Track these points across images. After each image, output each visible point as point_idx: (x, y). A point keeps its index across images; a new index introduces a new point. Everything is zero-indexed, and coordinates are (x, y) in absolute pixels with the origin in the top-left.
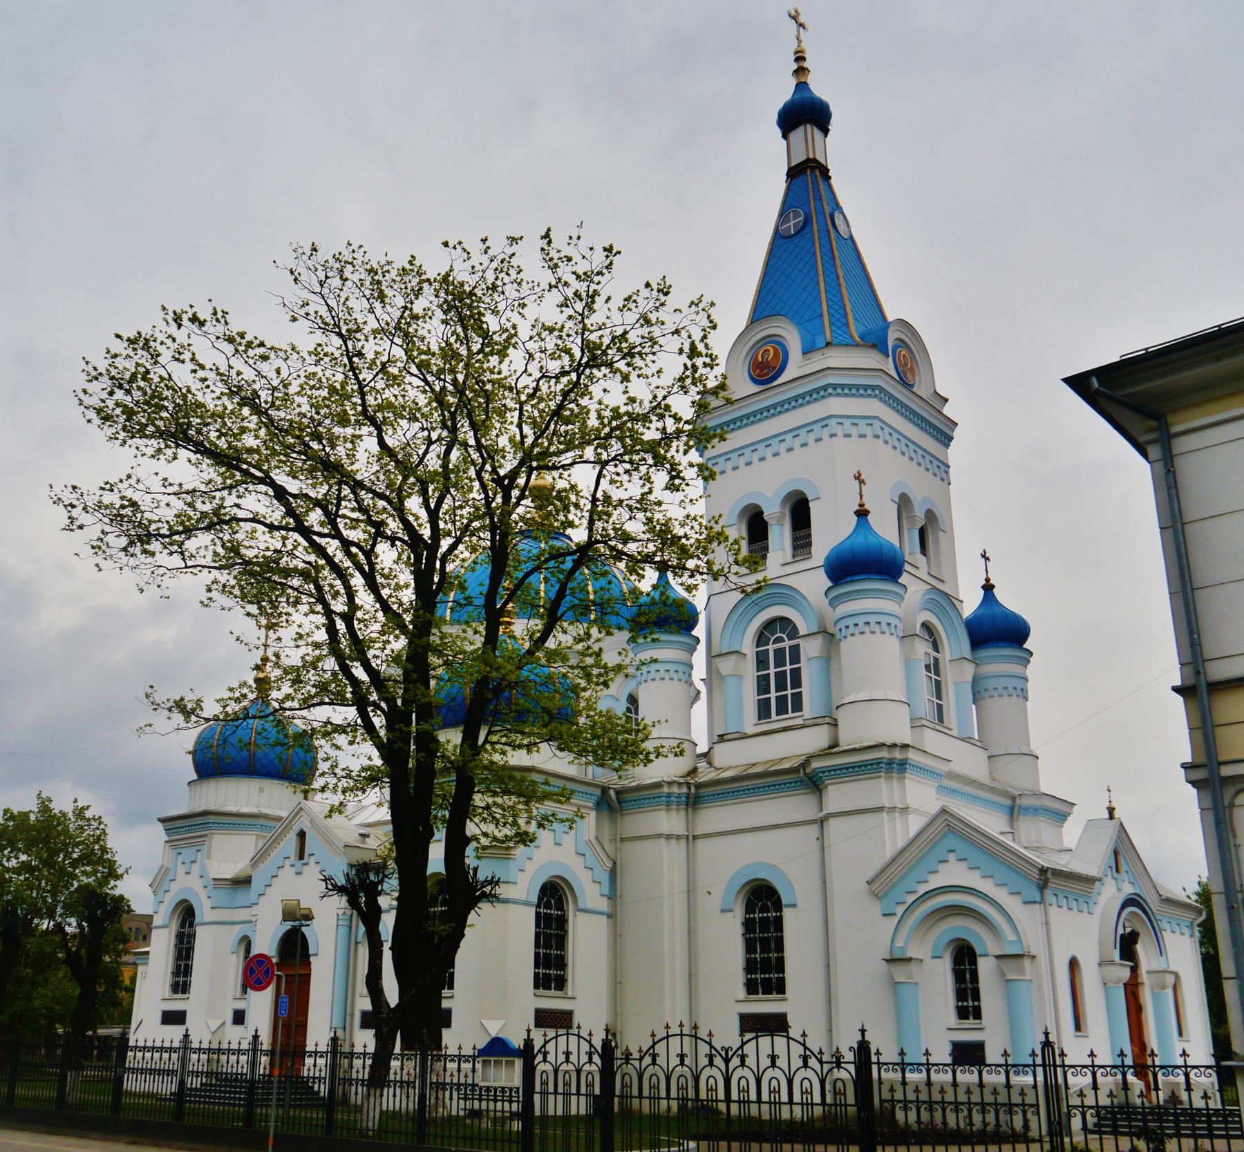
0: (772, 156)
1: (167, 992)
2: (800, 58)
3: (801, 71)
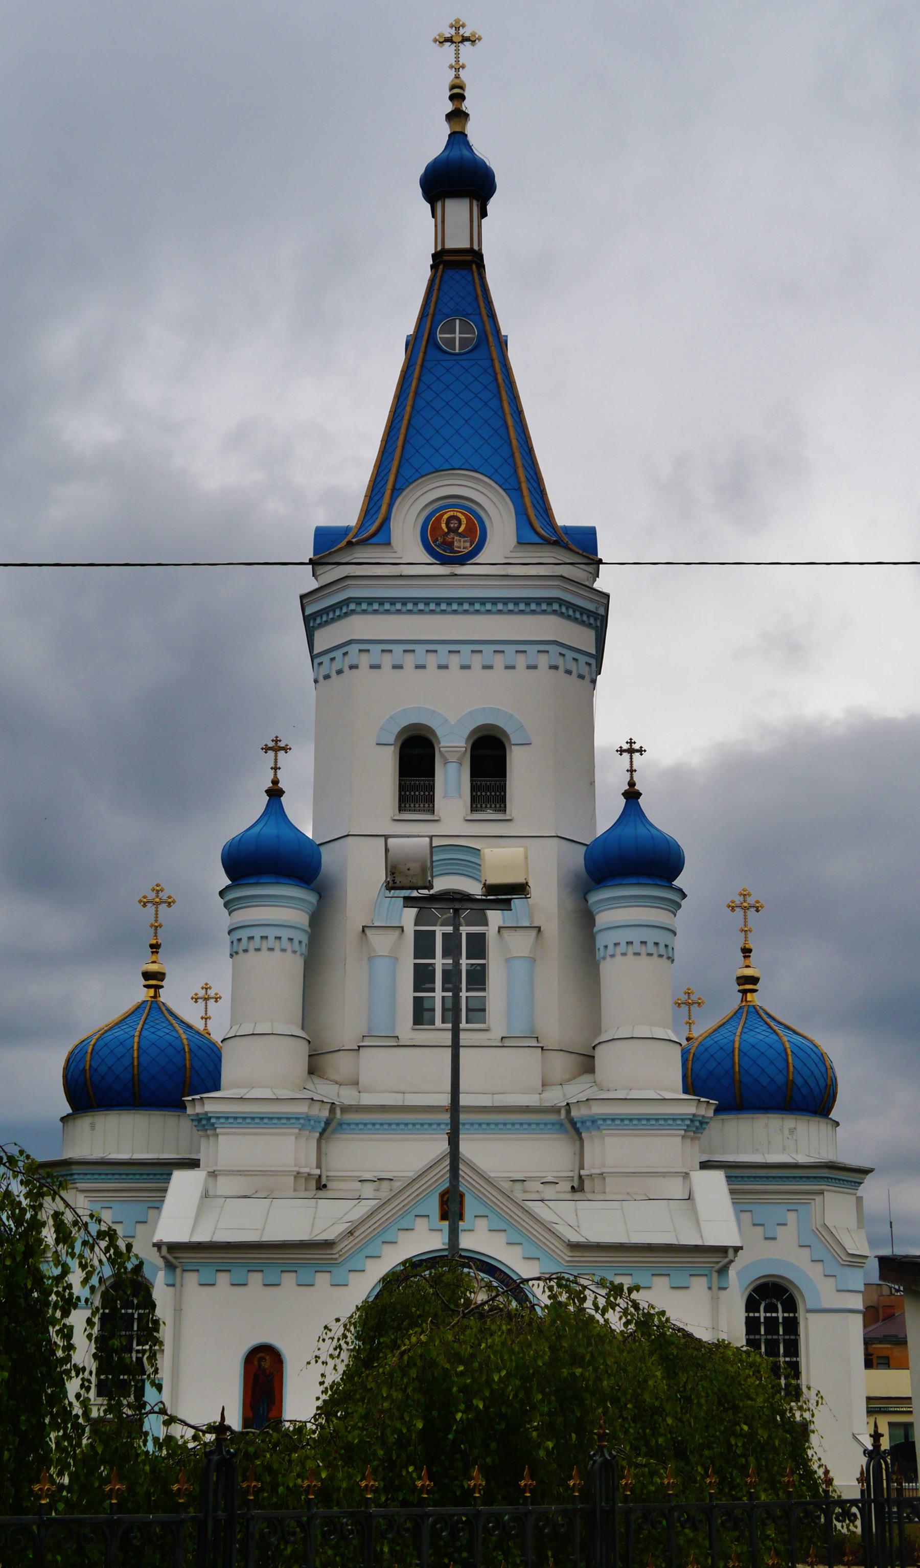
0: (416, 233)
1: (134, 1244)
2: (457, 96)
3: (457, 116)
